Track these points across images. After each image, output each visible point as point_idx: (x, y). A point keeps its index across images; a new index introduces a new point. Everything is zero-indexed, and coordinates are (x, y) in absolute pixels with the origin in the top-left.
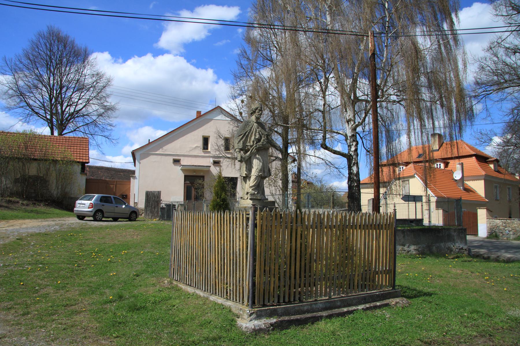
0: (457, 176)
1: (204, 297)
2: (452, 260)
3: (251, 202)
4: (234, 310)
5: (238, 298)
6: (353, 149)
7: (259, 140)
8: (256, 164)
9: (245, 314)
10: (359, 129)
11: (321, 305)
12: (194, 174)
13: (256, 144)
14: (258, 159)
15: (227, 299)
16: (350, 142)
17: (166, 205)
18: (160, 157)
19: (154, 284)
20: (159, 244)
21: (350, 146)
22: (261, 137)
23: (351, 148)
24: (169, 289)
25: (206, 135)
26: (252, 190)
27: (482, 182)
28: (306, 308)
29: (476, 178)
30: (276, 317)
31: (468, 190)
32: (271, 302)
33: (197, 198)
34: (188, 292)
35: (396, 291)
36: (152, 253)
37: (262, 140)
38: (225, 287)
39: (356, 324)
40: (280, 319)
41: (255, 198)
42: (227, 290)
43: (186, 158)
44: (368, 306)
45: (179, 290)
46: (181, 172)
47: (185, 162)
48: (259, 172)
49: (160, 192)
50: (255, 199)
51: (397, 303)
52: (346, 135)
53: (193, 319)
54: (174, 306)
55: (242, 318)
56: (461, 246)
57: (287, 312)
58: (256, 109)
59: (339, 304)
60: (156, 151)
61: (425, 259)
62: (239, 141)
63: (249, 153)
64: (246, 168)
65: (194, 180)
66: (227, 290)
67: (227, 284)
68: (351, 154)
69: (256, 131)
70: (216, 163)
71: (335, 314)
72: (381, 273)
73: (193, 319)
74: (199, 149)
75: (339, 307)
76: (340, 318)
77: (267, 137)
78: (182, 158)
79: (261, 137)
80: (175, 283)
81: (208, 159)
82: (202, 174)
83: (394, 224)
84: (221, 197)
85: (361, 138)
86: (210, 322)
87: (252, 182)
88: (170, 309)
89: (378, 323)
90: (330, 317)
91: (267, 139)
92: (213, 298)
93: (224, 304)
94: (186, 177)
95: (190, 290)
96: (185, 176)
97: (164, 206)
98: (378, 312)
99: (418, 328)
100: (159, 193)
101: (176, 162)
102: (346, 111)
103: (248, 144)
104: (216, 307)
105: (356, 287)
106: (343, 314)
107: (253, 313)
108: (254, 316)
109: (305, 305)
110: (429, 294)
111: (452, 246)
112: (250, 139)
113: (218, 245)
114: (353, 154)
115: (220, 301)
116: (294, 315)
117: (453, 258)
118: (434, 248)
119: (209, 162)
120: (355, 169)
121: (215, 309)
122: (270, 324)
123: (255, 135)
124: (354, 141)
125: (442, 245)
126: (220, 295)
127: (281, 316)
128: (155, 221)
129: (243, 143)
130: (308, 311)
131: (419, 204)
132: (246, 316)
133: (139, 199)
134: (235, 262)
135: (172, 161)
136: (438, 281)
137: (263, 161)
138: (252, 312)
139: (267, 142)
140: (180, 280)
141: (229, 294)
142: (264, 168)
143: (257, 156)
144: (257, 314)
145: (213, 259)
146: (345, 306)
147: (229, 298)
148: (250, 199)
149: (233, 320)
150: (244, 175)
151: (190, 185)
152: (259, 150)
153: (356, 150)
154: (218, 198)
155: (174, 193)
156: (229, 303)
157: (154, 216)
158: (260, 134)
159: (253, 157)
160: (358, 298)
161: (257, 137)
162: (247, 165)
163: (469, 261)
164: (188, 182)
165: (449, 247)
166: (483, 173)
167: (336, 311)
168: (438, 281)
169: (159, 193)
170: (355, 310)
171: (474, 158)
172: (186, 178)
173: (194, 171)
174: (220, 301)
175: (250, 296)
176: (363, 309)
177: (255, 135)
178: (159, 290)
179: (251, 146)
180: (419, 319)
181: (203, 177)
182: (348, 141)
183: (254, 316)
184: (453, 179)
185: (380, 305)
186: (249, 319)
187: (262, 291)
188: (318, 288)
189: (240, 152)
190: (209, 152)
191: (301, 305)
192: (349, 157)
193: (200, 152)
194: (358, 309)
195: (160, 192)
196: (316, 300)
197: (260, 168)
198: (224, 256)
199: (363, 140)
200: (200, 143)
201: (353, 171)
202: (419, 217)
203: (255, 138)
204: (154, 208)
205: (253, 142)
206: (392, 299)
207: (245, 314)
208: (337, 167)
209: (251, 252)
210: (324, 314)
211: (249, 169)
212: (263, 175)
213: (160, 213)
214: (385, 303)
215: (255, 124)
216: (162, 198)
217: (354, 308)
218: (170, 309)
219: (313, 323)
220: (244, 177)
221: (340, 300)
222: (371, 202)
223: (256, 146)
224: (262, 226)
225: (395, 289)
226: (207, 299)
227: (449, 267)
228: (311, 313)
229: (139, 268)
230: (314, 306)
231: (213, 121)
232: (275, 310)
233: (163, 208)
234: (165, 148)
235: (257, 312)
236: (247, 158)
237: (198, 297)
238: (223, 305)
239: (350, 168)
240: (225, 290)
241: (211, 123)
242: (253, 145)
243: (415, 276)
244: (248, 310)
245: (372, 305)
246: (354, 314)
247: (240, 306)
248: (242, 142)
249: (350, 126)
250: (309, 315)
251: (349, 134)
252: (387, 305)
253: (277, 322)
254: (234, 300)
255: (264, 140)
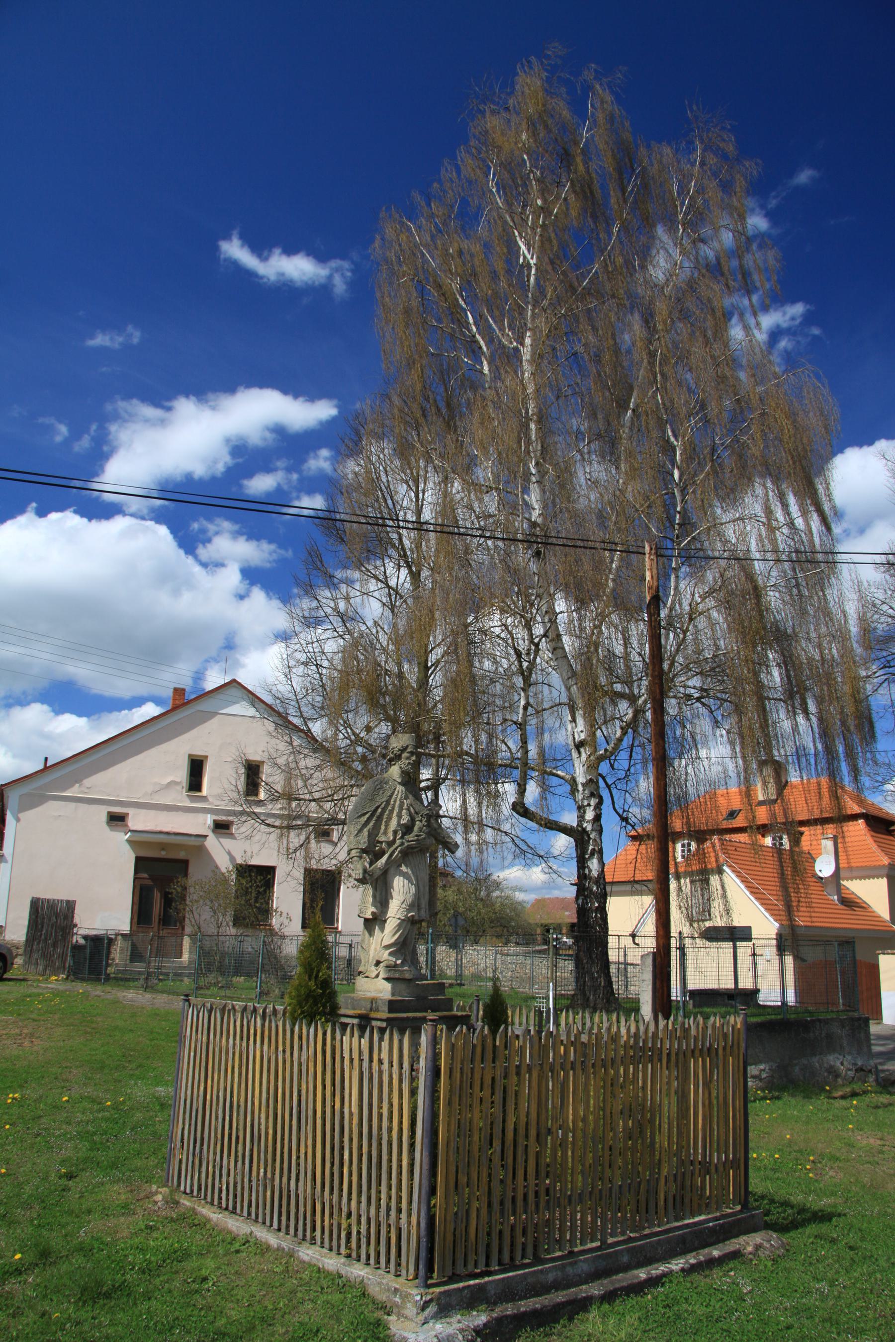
0: (825, 867)
1: (279, 1249)
2: (843, 1103)
3: (388, 986)
4: (374, 1290)
5: (385, 1255)
6: (590, 815)
7: (408, 829)
8: (402, 890)
9: (409, 1305)
10: (604, 768)
11: (585, 1267)
12: (163, 854)
13: (402, 838)
14: (405, 875)
15: (349, 1256)
16: (584, 799)
17: (85, 937)
18: (72, 805)
19: (126, 1206)
20: (102, 1068)
21: (581, 809)
22: (413, 820)
23: (584, 812)
24: (172, 1220)
25: (198, 752)
26: (390, 954)
27: (883, 883)
28: (551, 1277)
29: (868, 873)
30: (483, 1307)
31: (850, 903)
32: (470, 1267)
33: (166, 920)
34: (230, 1232)
35: (753, 1216)
36: (93, 1101)
37: (416, 829)
38: (344, 1225)
39: (678, 1316)
40: (495, 1315)
41: (397, 975)
42: (349, 1235)
43: (143, 812)
44: (693, 1261)
45: (201, 1224)
46: (127, 847)
47: (139, 821)
48: (408, 911)
49: (74, 902)
50: (398, 979)
51: (758, 1247)
52: (574, 780)
53: (267, 1321)
54: (205, 1279)
55: (400, 1315)
56: (860, 1063)
57: (509, 1293)
58: (404, 750)
59: (625, 1259)
60: (64, 790)
61: (779, 1103)
62: (360, 831)
63: (383, 860)
64: (374, 896)
65: (162, 874)
66: (349, 1235)
67: (349, 1215)
68: (584, 829)
69: (402, 804)
70: (221, 827)
71: (622, 1289)
72: (573, 1068)
73: (267, 1321)
74: (179, 788)
75: (626, 1268)
76: (633, 1301)
77: (428, 821)
78: (131, 811)
79: (413, 820)
80: (186, 1202)
81: (200, 817)
82: (182, 855)
83: (743, 1045)
84: (317, 976)
85: (608, 786)
86: (318, 1331)
87: (388, 934)
88: (196, 1291)
89: (730, 1311)
90: (609, 1297)
91: (429, 825)
92: (308, 1253)
93: (343, 1272)
94: (139, 860)
95: (236, 1225)
96: (138, 859)
97: (82, 941)
98: (718, 1278)
99: (828, 1325)
100: (70, 906)
101: (116, 820)
102: (574, 720)
103: (382, 838)
104: (324, 1283)
105: (661, 1211)
106: (638, 1288)
107: (431, 1300)
108: (432, 1309)
109: (548, 1270)
110: (822, 1217)
111: (838, 1064)
112: (387, 826)
113: (324, 1112)
114: (589, 828)
115: (332, 1262)
116: (525, 1298)
117: (843, 1097)
118: (797, 1069)
119: (198, 824)
120: (594, 865)
121: (322, 1288)
122: (475, 1330)
123: (400, 816)
124: (592, 795)
125: (815, 1061)
126: (327, 1244)
127: (495, 1304)
128: (56, 982)
129: (369, 836)
130: (557, 1286)
131: (744, 949)
132: (410, 1310)
133: (10, 916)
134: (374, 1160)
135: (104, 817)
136: (831, 1173)
137: (417, 880)
138: (429, 1297)
139: (429, 834)
140: (201, 1192)
141: (354, 1245)
142: (419, 899)
143: (404, 868)
144: (438, 1304)
145: (309, 1149)
146: (639, 1265)
147: (354, 1255)
148: (387, 979)
149: (378, 1323)
150: (369, 916)
151: (149, 882)
152: (407, 854)
153: (597, 818)
154: (310, 979)
155: (106, 908)
156: (358, 1271)
157: (51, 968)
158: (410, 815)
159: (392, 871)
160: (668, 1241)
161: (405, 820)
162: (375, 889)
163: (886, 1106)
164: (145, 875)
165: (832, 1067)
166: (886, 861)
167: (621, 1279)
168: (831, 1173)
169: (70, 906)
170: (664, 1275)
171: (860, 821)
172: (140, 862)
173: (163, 846)
174: (332, 1262)
175: (423, 1254)
176: (683, 1270)
177: (400, 816)
178: (148, 1227)
179: (390, 844)
180: (824, 1298)
181: (185, 863)
182: (580, 796)
183: (432, 1309)
184: (815, 875)
185: (720, 1257)
186: (421, 1318)
187: (450, 1237)
188: (576, 1220)
189: (360, 857)
190: (204, 799)
191: (541, 1271)
192: (579, 836)
193: (180, 797)
194: (672, 1271)
195: (74, 902)
196: (571, 1253)
197: (410, 898)
198: (342, 1142)
199: (614, 791)
200: (182, 775)
201: (590, 871)
202: (746, 983)
203: (399, 824)
204: (55, 945)
205: (395, 832)
206: (745, 1237)
207: (409, 1305)
208: (542, 853)
209: (426, 1141)
210: (595, 1289)
211: (382, 900)
212: (416, 918)
213: (69, 961)
214: (732, 1249)
215: (400, 788)
216: (77, 920)
217: (662, 1268)
218: (196, 1291)
219: (571, 1319)
220: (366, 920)
221: (628, 1250)
222: (649, 961)
223: (402, 844)
224: (451, 1070)
225: (749, 1210)
226: (291, 1254)
227: (848, 1129)
228: (564, 1289)
229: (68, 1151)
230: (570, 1270)
231: (216, 720)
232: (481, 1288)
233: (77, 948)
234: (87, 782)
235: (439, 1299)
236: (378, 873)
237: (264, 1249)
238: (340, 1276)
239: (582, 863)
240: (343, 1234)
241: (213, 724)
242: (394, 841)
243: (776, 1160)
244: (416, 1294)
245: (702, 1258)
246: (663, 1284)
247: (390, 1280)
248: (365, 832)
249: (584, 756)
250: (560, 1297)
251: (581, 779)
252: (736, 1255)
253: (488, 1322)
254: (372, 1261)
255: (420, 830)
